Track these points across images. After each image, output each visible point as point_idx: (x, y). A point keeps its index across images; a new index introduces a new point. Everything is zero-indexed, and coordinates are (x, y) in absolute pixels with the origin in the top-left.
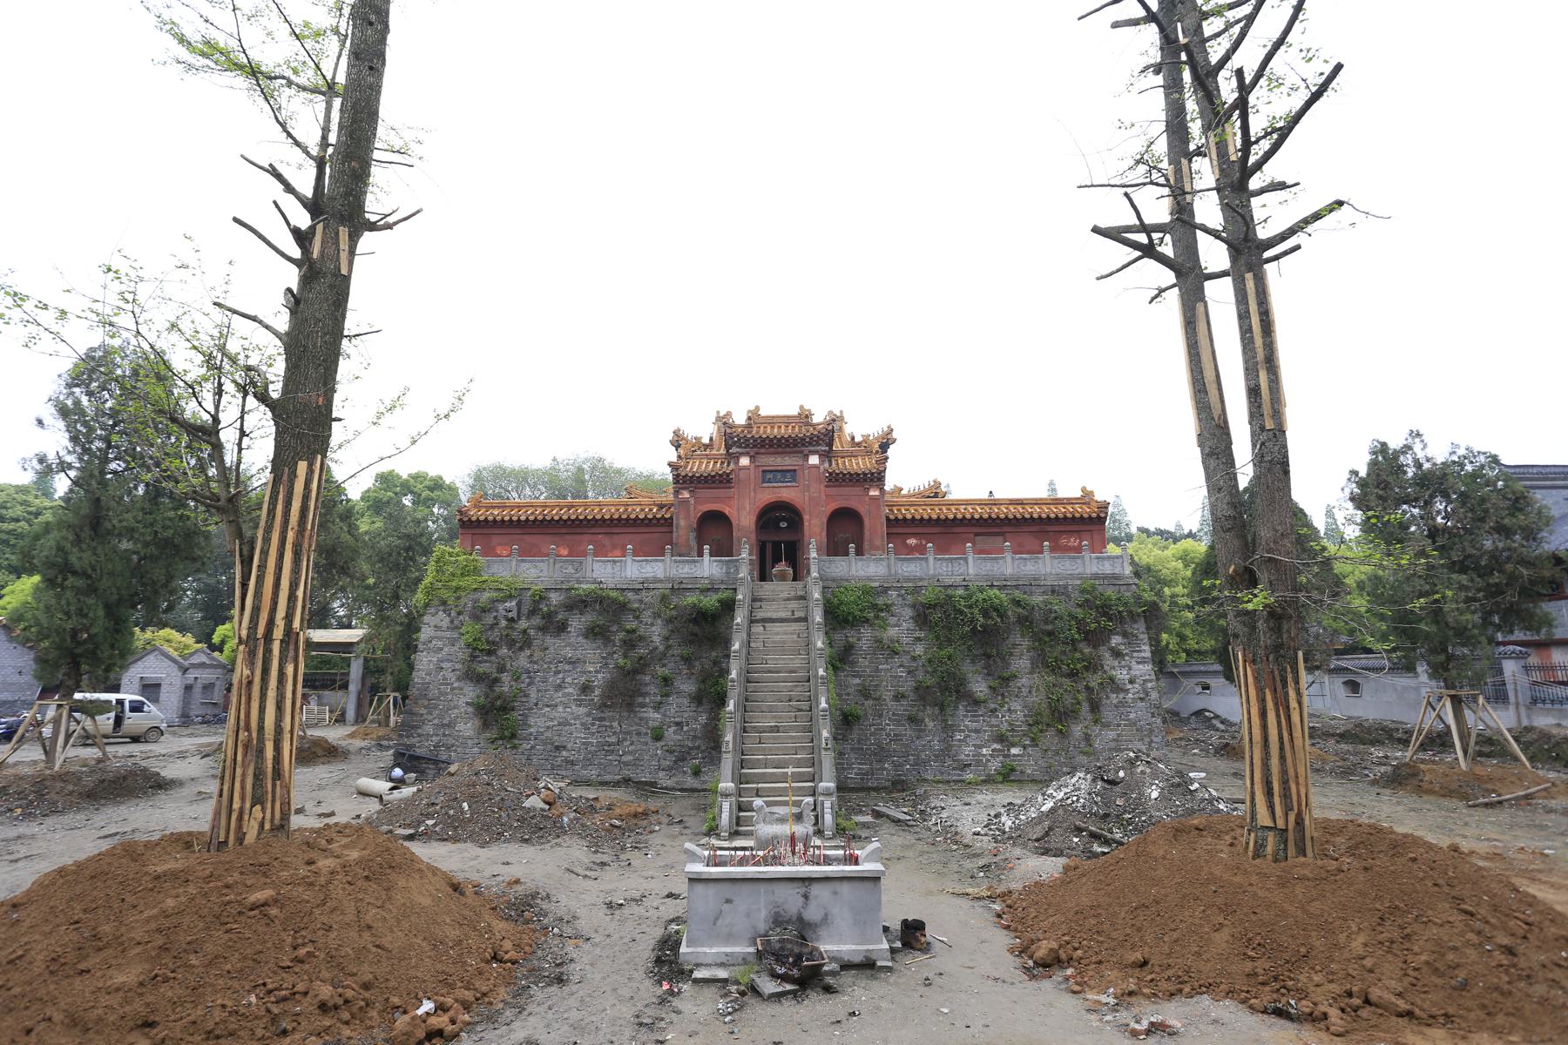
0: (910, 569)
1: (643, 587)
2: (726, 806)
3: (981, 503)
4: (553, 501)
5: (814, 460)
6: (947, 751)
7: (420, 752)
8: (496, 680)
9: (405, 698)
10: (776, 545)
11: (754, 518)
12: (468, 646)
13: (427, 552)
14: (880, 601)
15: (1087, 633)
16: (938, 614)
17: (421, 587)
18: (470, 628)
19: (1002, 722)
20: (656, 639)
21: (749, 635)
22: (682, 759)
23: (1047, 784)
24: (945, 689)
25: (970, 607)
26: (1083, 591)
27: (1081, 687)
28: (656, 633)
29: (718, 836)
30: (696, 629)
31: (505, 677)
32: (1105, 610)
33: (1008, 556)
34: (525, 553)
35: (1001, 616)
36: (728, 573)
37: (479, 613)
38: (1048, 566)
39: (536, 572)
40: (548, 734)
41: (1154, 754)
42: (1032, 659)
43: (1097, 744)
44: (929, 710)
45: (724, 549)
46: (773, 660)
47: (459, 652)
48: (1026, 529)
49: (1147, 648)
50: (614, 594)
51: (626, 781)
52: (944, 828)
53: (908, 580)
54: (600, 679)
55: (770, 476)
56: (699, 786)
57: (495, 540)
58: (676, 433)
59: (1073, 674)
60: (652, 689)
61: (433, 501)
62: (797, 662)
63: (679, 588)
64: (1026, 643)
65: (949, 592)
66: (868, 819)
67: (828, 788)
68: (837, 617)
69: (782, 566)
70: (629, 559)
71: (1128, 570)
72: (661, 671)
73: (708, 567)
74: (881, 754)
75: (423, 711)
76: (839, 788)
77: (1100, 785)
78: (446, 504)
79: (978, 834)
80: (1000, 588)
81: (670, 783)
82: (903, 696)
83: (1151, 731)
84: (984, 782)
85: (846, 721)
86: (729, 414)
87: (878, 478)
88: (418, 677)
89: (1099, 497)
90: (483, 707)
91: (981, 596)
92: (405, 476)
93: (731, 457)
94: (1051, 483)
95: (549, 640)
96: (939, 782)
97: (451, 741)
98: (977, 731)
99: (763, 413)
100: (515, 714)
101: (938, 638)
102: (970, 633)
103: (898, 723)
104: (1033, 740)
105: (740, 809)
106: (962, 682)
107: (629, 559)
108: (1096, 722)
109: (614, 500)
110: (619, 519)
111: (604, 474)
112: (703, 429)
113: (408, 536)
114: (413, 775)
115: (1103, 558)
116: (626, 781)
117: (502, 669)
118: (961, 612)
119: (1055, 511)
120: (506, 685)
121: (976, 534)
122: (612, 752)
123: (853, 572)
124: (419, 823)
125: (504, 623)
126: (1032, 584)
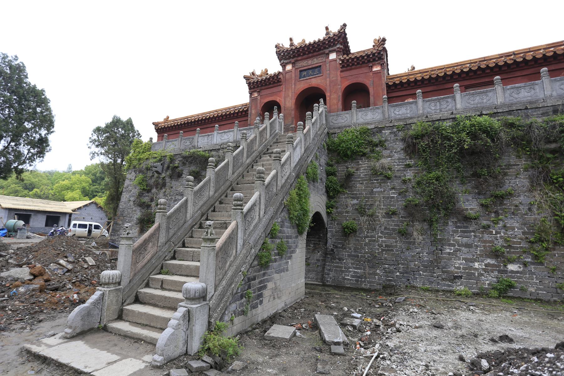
6: (435, 263)
14: (375, 139)
16: (423, 145)
24: (433, 206)
44: (418, 225)
48: (518, 74)
53: (400, 120)
55: (305, 73)
74: (374, 261)
80: (491, 115)
82: (394, 213)
95: (174, 183)
103: (389, 236)
104: (536, 257)
106: (451, 199)
123: (355, 120)
126: (527, 108)
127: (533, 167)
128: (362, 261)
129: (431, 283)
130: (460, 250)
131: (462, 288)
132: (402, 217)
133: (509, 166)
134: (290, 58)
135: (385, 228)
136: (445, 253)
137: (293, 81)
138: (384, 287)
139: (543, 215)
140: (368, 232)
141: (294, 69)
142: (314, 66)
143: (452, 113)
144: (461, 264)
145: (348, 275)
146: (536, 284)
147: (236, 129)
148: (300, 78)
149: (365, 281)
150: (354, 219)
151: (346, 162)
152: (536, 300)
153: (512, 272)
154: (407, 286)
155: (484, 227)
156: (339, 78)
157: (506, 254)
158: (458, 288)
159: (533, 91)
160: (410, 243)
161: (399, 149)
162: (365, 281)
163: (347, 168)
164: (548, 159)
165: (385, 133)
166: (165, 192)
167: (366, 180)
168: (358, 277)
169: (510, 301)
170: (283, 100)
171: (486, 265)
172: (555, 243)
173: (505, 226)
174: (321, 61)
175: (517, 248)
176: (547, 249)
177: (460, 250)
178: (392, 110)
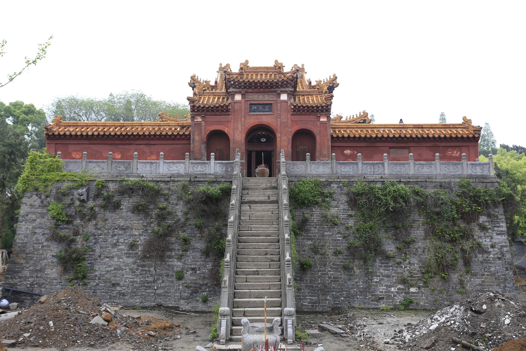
0: (346, 170)
1: (170, 180)
2: (224, 322)
3: (394, 127)
4: (110, 122)
5: (284, 97)
6: (368, 289)
7: (19, 288)
8: (73, 241)
9: (9, 253)
10: (258, 153)
11: (244, 135)
12: (53, 218)
13: (24, 155)
14: (326, 191)
15: (463, 214)
16: (364, 200)
17: (20, 179)
18: (54, 207)
19: (405, 271)
20: (179, 214)
21: (240, 212)
22: (195, 292)
23: (434, 312)
24: (367, 248)
25: (385, 195)
26: (462, 186)
27: (458, 249)
28: (179, 210)
29: (218, 342)
30: (205, 208)
31: (79, 239)
32: (476, 199)
33: (411, 162)
34: (92, 156)
35: (405, 202)
36: (226, 171)
37: (60, 196)
38: (438, 169)
39: (99, 169)
40: (108, 276)
41: (507, 294)
42: (425, 230)
43: (468, 287)
44: (357, 262)
45: (224, 155)
46: (256, 228)
47: (47, 222)
49: (504, 224)
50: (151, 184)
51: (159, 306)
52: (366, 339)
53: (345, 177)
54: (142, 240)
55: (255, 107)
56: (207, 310)
57: (71, 148)
58: (193, 78)
59: (453, 241)
60: (176, 247)
61: (28, 122)
62: (271, 230)
63: (194, 181)
64: (422, 220)
65: (372, 185)
66: (316, 331)
67: (290, 312)
68: (298, 201)
69: (262, 168)
70: (161, 161)
71: (493, 173)
72: (182, 235)
73: (214, 167)
74: (325, 290)
75: (22, 261)
76: (298, 312)
77: (469, 313)
78: (37, 124)
79: (388, 343)
80: (406, 183)
81: (188, 307)
83: (505, 280)
84: (392, 309)
85: (302, 268)
86: (228, 66)
87: (326, 109)
88: (19, 239)
89: (475, 123)
90: (64, 258)
91: (392, 189)
92: (7, 104)
93: (229, 95)
94: (442, 115)
95: (108, 214)
96: (362, 309)
97: (42, 281)
98: (388, 276)
99: (250, 65)
100: (85, 263)
101: (363, 215)
102: (385, 213)
103: (336, 270)
104: (425, 283)
105: (233, 324)
106: (379, 244)
107: (161, 161)
108: (467, 272)
109: (152, 122)
110: (155, 135)
111: (144, 105)
112: (211, 76)
113: (10, 145)
114: (15, 304)
115: (476, 165)
116: (159, 306)
117: (76, 233)
118: (379, 199)
119: (448, 132)
120: (79, 243)
121: (391, 148)
122: (150, 287)
123: (309, 171)
124: (19, 336)
125: (77, 203)
126: (426, 181)
127: (427, 223)
128: (316, 290)
129: (365, 303)
130: (383, 280)
131: (384, 305)
132: (345, 256)
133: (414, 221)
134: (240, 87)
135: (333, 264)
136: (374, 282)
137: (243, 114)
138: (332, 309)
139: (430, 255)
140: (320, 267)
141: (244, 100)
142: (264, 102)
143: (382, 178)
144: (383, 289)
145: (305, 302)
146: (424, 299)
147: (188, 162)
148: (250, 112)
149: (318, 306)
150: (310, 257)
151: (302, 208)
152: (424, 310)
153: (412, 293)
154: (349, 307)
155: (398, 263)
156: (290, 122)
157: (410, 281)
158: (381, 306)
159: (430, 169)
160: (351, 275)
161: (343, 202)
162: (318, 306)
163: (304, 214)
164: (435, 219)
165: (334, 187)
166: (96, 224)
167: (318, 225)
168: (313, 303)
169: (410, 311)
170: (232, 132)
171: (398, 289)
172: (435, 274)
173: (410, 263)
174: (271, 99)
175: (415, 277)
176: (431, 277)
177: (383, 280)
178: (339, 166)
